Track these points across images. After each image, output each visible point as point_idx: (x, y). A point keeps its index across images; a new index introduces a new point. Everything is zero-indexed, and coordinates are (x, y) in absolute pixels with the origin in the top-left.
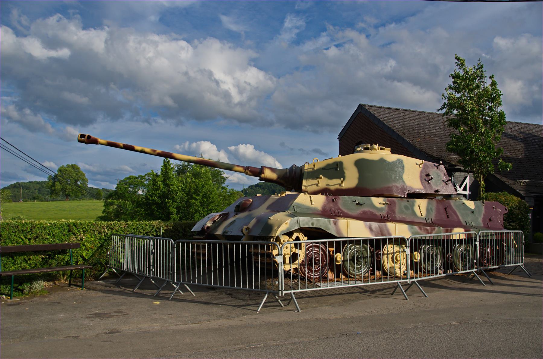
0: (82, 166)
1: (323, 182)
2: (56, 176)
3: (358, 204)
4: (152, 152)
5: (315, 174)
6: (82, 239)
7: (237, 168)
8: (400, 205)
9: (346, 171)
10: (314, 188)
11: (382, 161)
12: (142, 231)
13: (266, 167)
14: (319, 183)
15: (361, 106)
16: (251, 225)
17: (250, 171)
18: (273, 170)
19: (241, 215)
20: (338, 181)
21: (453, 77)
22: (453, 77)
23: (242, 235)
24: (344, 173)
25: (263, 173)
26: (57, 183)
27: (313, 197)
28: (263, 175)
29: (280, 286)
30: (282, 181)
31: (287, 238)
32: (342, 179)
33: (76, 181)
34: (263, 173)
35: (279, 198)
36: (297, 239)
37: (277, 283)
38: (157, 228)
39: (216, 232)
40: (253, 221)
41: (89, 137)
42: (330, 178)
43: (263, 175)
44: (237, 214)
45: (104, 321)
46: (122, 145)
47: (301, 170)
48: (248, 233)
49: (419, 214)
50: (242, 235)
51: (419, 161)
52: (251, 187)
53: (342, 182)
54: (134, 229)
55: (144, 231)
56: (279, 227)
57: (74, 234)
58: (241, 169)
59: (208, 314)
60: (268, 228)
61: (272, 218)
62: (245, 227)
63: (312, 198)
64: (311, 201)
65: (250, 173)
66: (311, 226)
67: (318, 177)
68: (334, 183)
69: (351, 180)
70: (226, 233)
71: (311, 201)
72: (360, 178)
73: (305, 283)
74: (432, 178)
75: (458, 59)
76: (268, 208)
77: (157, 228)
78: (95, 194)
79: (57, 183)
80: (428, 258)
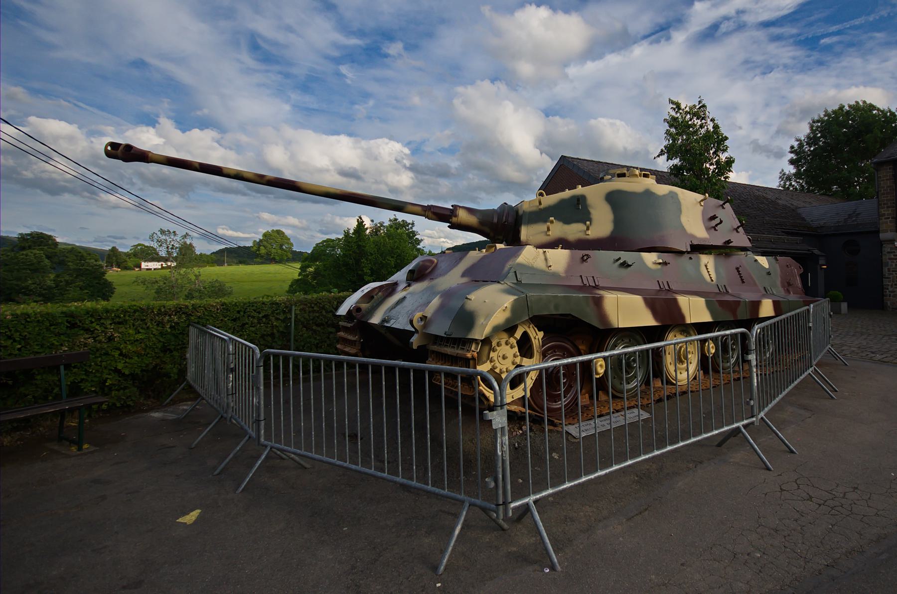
0: (288, 232)
1: (558, 229)
2: (261, 241)
4: (258, 179)
5: (540, 216)
6: (111, 339)
7: (410, 208)
9: (591, 211)
10: (544, 239)
11: (648, 193)
12: (256, 314)
13: (460, 207)
14: (548, 229)
15: (563, 158)
16: (429, 311)
17: (434, 213)
18: (470, 211)
20: (580, 227)
24: (589, 213)
25: (456, 216)
26: (262, 248)
27: (550, 252)
28: (454, 219)
29: (500, 492)
30: (487, 230)
31: (504, 337)
32: (588, 223)
33: (281, 246)
34: (456, 216)
35: (484, 257)
36: (525, 335)
37: (492, 485)
38: (286, 307)
39: (370, 318)
40: (436, 302)
41: (129, 147)
42: (567, 221)
43: (454, 219)
44: (409, 285)
46: (197, 166)
47: (517, 212)
48: (425, 327)
50: (413, 330)
51: (700, 197)
53: (588, 229)
54: (239, 312)
55: (259, 313)
56: (488, 317)
57: (87, 330)
58: (419, 209)
60: (467, 319)
61: (472, 296)
62: (418, 315)
63: (548, 254)
64: (546, 259)
65: (434, 217)
66: (554, 313)
67: (545, 220)
68: (574, 231)
69: (602, 223)
70: (388, 322)
71: (546, 259)
72: (617, 222)
73: (543, 431)
74: (721, 222)
75: (672, 102)
76: (463, 275)
77: (286, 307)
78: (297, 256)
79: (262, 248)
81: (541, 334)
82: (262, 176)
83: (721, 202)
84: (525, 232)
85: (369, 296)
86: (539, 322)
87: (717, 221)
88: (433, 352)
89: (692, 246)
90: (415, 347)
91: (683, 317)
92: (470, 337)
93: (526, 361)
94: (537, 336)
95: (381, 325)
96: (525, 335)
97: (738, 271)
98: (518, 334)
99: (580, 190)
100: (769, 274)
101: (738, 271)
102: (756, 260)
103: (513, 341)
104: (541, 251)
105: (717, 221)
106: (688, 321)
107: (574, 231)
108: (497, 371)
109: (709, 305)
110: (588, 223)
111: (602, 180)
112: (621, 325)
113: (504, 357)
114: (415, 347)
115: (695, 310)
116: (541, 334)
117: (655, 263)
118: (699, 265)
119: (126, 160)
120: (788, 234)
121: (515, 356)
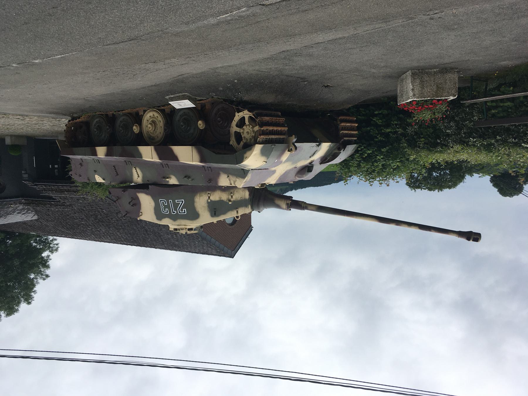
3: (189, 177)
8: (153, 177)
19: (306, 162)
21: (47, 276)
22: (47, 276)
23: (296, 144)
28: (289, 202)
32: (209, 201)
36: (239, 143)
39: (330, 145)
41: (469, 239)
44: (310, 163)
45: (257, 68)
49: (138, 170)
50: (296, 144)
52: (291, 190)
58: (309, 207)
59: (310, 55)
64: (230, 180)
68: (216, 196)
72: (193, 202)
74: (129, 203)
80: (128, 128)
81: (237, 114)
82: (397, 225)
83: (128, 215)
84: (246, 195)
85: (335, 156)
86: (232, 150)
87: (131, 204)
88: (284, 134)
89: (148, 188)
90: (294, 136)
91: (156, 150)
92: (262, 145)
93: (238, 130)
94: (233, 141)
95: (319, 142)
96: (239, 143)
97: (117, 173)
98: (242, 143)
99: (215, 220)
100: (95, 171)
101: (117, 173)
102: (104, 179)
103: (244, 141)
104: (233, 185)
105: (131, 204)
106: (152, 147)
107: (216, 196)
108: (251, 126)
109: (140, 156)
110: (209, 201)
111: (202, 227)
112: (190, 148)
113: (248, 132)
114: (294, 136)
115: (148, 154)
116: (231, 143)
117: (170, 178)
118: (143, 177)
119: (471, 233)
120: (51, 198)
121: (243, 133)
